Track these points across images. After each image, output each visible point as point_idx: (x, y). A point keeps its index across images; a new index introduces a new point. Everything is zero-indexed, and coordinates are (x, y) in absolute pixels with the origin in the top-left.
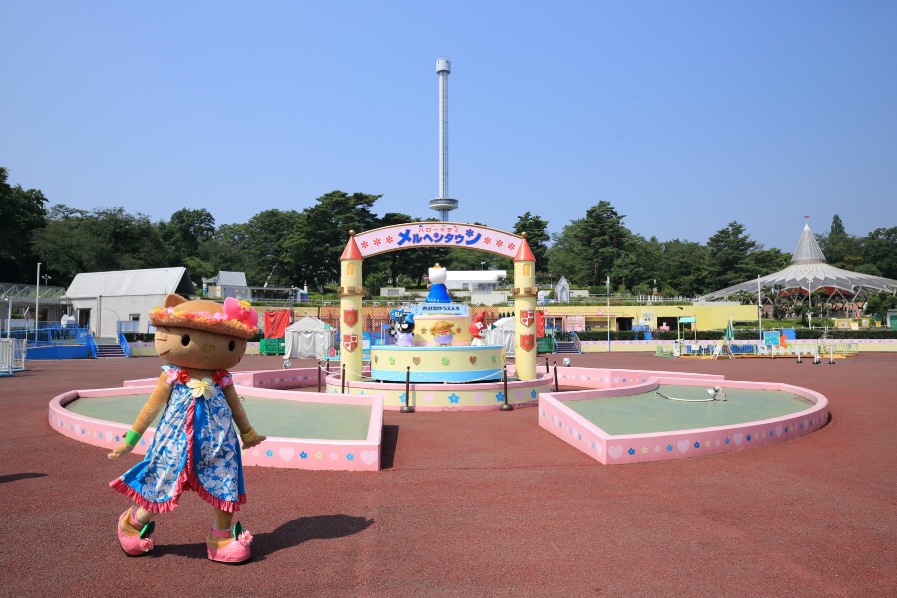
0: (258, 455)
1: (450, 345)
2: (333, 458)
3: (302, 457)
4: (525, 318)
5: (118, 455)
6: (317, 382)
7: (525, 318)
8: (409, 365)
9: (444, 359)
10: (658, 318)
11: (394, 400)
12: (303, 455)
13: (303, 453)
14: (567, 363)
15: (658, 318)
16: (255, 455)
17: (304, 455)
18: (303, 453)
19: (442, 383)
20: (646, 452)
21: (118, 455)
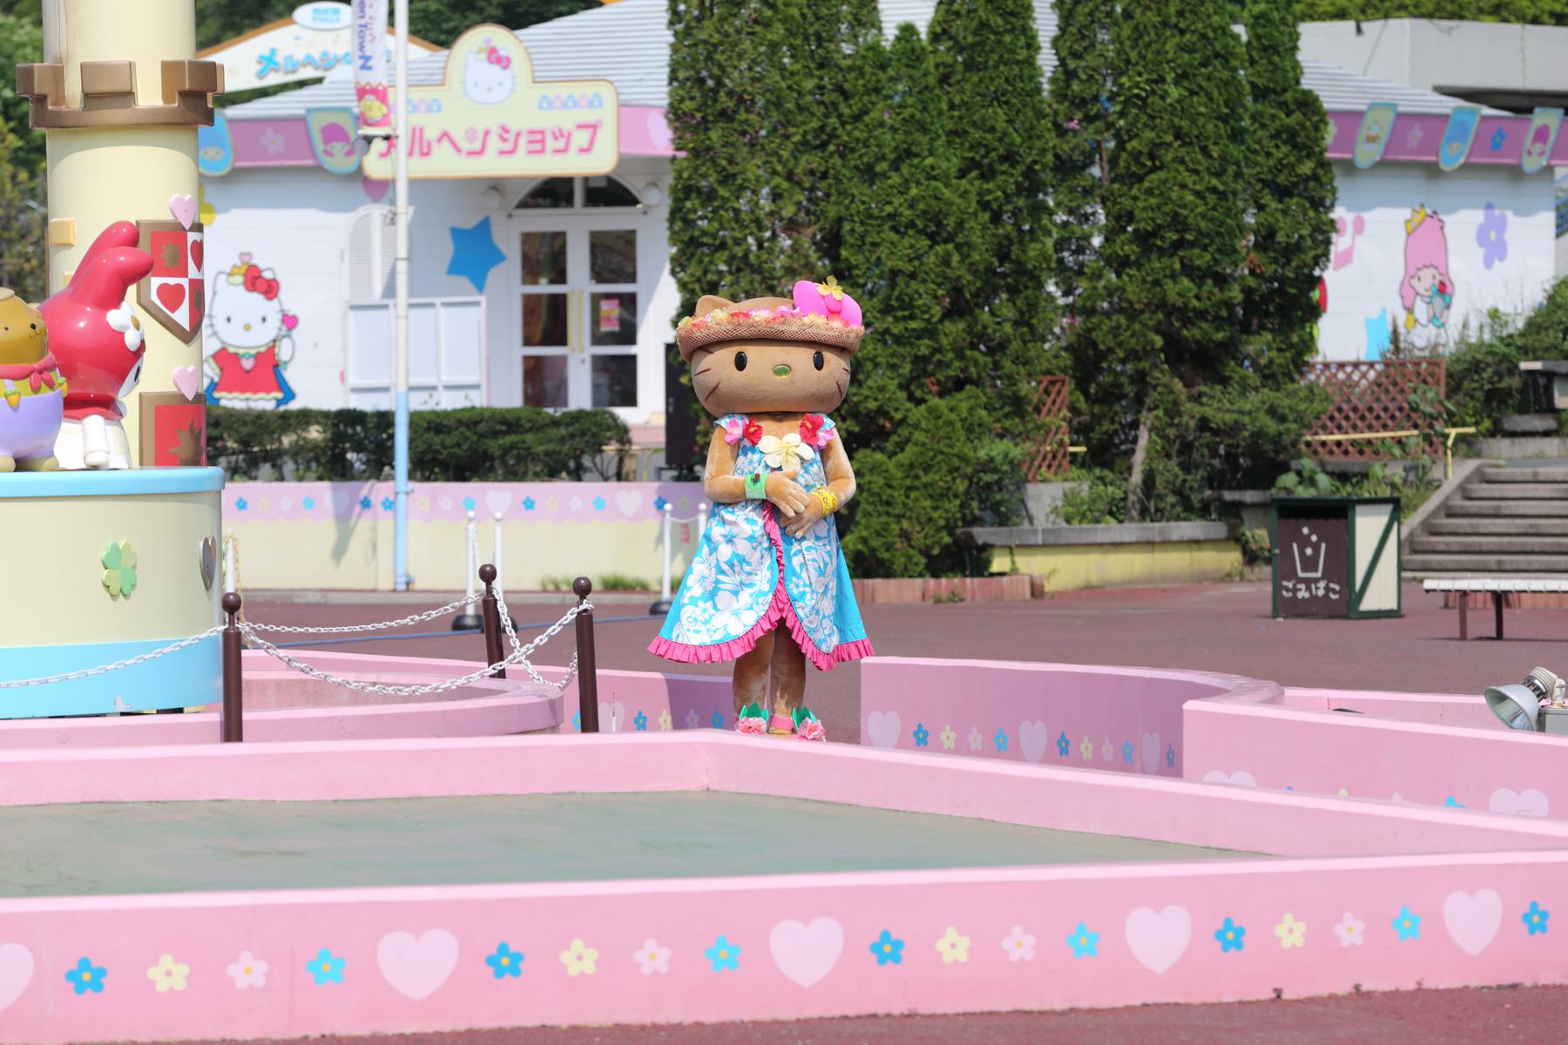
0: (1359, 940)
1: (338, 20)
2: (162, 985)
3: (499, 973)
4: (172, 281)
5: (1194, 346)
6: (60, 241)
7: (172, 281)
8: (249, 322)
9: (475, 133)
10: (633, 232)
11: (1538, 13)
12: (86, 976)
13: (885, 936)
14: (1234, 167)
15: (633, 232)
16: (574, 969)
17: (504, 962)
18: (885, 936)
19: (180, 711)
20: (1028, 955)
21: (1194, 346)
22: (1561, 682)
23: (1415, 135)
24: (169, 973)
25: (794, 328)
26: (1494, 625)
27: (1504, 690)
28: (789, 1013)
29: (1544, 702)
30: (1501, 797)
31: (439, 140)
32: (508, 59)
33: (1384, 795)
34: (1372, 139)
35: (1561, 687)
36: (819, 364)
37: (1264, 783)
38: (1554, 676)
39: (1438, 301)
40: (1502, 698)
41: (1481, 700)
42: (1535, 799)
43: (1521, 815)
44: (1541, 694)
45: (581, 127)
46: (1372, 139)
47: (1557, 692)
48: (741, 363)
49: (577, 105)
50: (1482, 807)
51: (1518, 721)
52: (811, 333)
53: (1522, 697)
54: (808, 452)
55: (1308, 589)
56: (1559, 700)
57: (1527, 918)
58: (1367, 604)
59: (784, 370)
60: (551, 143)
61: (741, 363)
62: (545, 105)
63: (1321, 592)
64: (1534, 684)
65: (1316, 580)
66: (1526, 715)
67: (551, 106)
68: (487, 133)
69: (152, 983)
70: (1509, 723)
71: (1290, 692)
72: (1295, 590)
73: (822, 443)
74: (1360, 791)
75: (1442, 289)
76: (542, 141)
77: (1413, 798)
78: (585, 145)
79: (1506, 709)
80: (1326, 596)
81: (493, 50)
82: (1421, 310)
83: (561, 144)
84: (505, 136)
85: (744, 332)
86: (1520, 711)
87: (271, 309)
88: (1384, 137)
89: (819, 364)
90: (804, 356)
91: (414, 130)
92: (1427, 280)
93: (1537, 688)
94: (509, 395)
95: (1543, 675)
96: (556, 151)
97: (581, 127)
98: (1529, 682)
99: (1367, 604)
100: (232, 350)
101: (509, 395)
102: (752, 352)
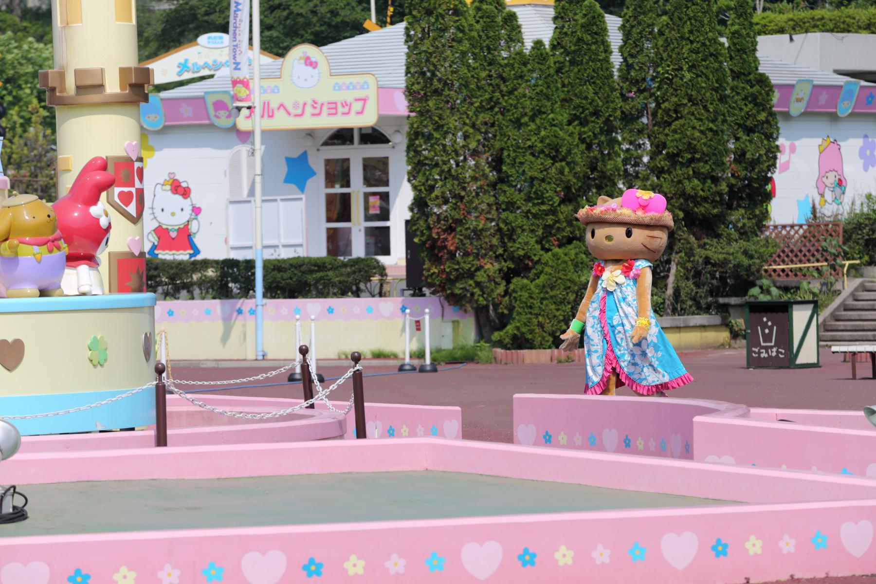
23: (824, 97)
31: (279, 108)
32: (316, 63)
33: (805, 467)
34: (799, 100)
36: (629, 234)
39: (838, 190)
45: (357, 100)
46: (799, 100)
49: (355, 88)
55: (767, 352)
58: (800, 360)
60: (340, 109)
62: (337, 88)
63: (774, 354)
65: (771, 347)
67: (340, 89)
68: (305, 104)
71: (753, 410)
72: (759, 353)
75: (840, 183)
76: (336, 108)
78: (360, 110)
80: (777, 356)
81: (308, 58)
82: (829, 195)
83: (346, 110)
84: (315, 105)
87: (186, 204)
88: (806, 98)
89: (629, 234)
90: (619, 232)
91: (264, 103)
92: (832, 179)
94: (319, 250)
96: (343, 114)
97: (357, 100)
99: (800, 360)
100: (164, 227)
101: (319, 250)
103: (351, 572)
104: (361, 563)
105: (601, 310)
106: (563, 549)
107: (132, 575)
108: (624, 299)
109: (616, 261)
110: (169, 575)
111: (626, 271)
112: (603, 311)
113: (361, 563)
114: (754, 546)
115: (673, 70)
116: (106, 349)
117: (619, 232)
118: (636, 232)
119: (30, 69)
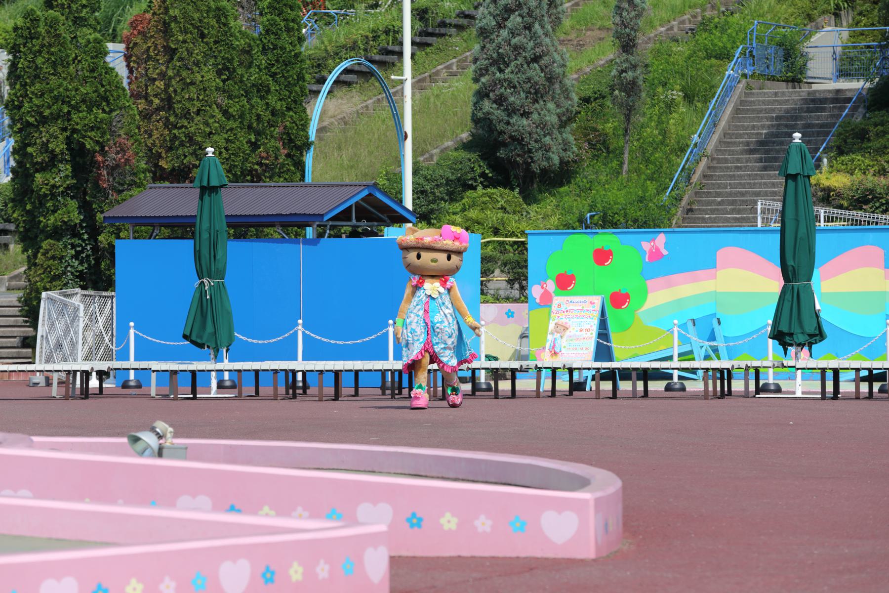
12: (415, 521)
22: (170, 429)
24: (449, 522)
25: (439, 245)
26: (253, 389)
27: (140, 435)
28: (550, 554)
29: (161, 441)
30: (184, 500)
33: (112, 501)
35: (171, 432)
36: (449, 258)
37: (38, 496)
38: (167, 426)
40: (136, 440)
41: (125, 440)
42: (204, 500)
43: (195, 509)
44: (160, 437)
47: (169, 435)
48: (419, 257)
50: (172, 505)
51: (147, 452)
52: (446, 247)
53: (149, 438)
54: (442, 290)
56: (170, 440)
57: (263, 575)
59: (433, 261)
61: (419, 257)
64: (156, 431)
66: (152, 448)
69: (442, 526)
70: (141, 454)
71: (36, 439)
73: (449, 287)
74: (98, 498)
77: (128, 502)
79: (139, 446)
85: (420, 245)
86: (148, 446)
89: (449, 258)
90: (443, 257)
93: (158, 434)
95: (161, 426)
98: (153, 430)
102: (423, 254)
103: (446, 527)
104: (455, 520)
105: (425, 310)
106: (448, 516)
107: (173, 584)
108: (443, 304)
109: (433, 277)
110: (168, 590)
111: (443, 284)
112: (426, 311)
113: (455, 520)
114: (449, 522)
115: (132, 109)
116: (693, 321)
117: (443, 257)
118: (453, 257)
119: (67, 100)
